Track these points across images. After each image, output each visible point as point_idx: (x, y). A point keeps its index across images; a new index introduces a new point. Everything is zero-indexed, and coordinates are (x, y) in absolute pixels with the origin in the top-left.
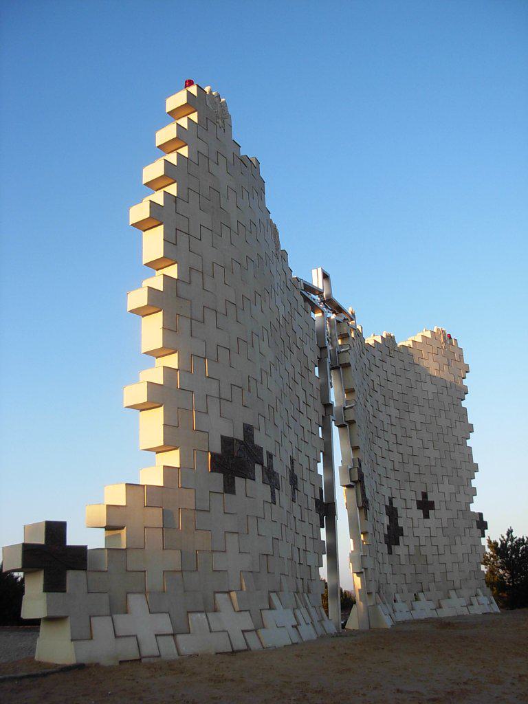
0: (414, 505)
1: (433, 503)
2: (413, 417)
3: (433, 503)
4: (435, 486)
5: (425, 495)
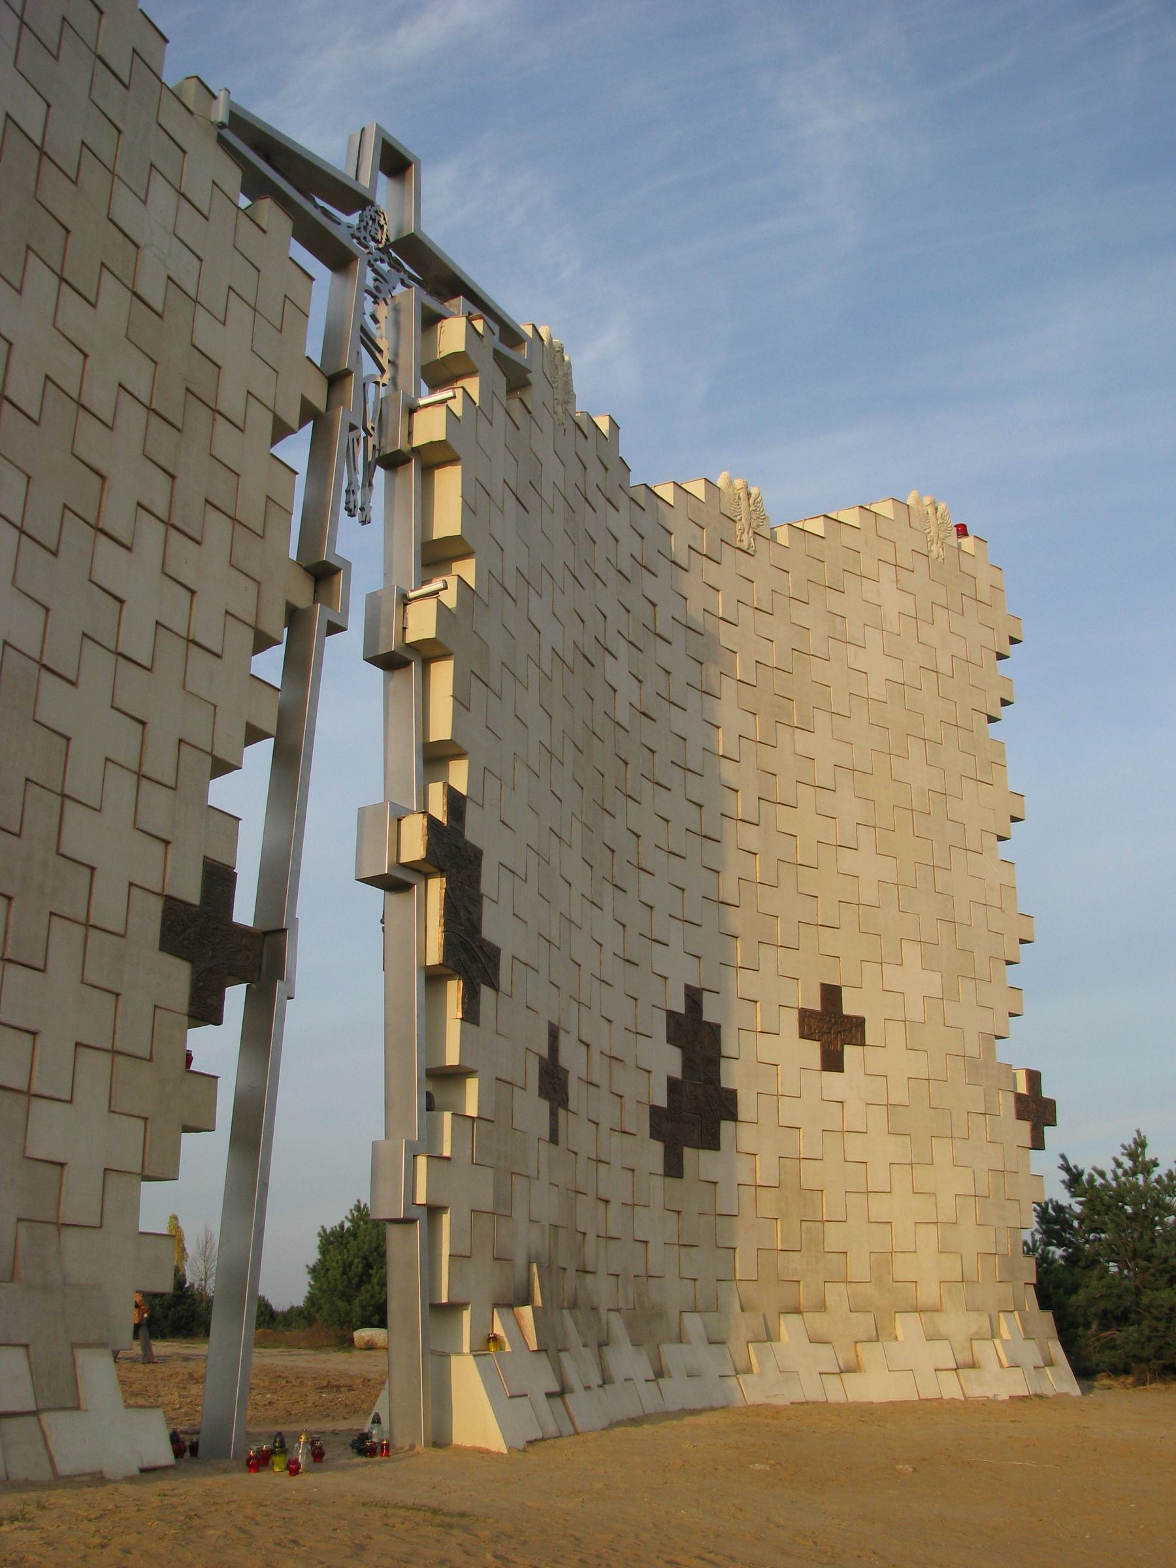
0: (790, 1022)
1: (859, 1023)
3: (859, 1023)
5: (831, 994)
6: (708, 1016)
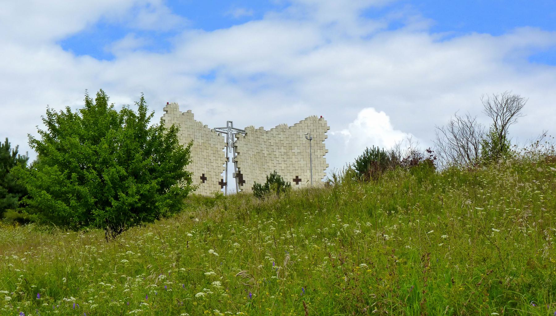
2: (293, 151)
4: (302, 174)
6: (205, 176)
